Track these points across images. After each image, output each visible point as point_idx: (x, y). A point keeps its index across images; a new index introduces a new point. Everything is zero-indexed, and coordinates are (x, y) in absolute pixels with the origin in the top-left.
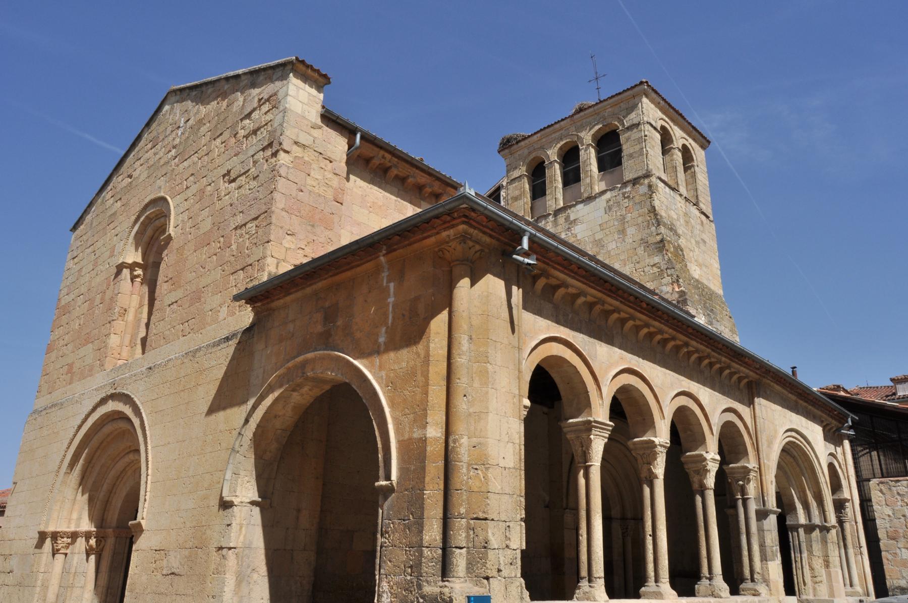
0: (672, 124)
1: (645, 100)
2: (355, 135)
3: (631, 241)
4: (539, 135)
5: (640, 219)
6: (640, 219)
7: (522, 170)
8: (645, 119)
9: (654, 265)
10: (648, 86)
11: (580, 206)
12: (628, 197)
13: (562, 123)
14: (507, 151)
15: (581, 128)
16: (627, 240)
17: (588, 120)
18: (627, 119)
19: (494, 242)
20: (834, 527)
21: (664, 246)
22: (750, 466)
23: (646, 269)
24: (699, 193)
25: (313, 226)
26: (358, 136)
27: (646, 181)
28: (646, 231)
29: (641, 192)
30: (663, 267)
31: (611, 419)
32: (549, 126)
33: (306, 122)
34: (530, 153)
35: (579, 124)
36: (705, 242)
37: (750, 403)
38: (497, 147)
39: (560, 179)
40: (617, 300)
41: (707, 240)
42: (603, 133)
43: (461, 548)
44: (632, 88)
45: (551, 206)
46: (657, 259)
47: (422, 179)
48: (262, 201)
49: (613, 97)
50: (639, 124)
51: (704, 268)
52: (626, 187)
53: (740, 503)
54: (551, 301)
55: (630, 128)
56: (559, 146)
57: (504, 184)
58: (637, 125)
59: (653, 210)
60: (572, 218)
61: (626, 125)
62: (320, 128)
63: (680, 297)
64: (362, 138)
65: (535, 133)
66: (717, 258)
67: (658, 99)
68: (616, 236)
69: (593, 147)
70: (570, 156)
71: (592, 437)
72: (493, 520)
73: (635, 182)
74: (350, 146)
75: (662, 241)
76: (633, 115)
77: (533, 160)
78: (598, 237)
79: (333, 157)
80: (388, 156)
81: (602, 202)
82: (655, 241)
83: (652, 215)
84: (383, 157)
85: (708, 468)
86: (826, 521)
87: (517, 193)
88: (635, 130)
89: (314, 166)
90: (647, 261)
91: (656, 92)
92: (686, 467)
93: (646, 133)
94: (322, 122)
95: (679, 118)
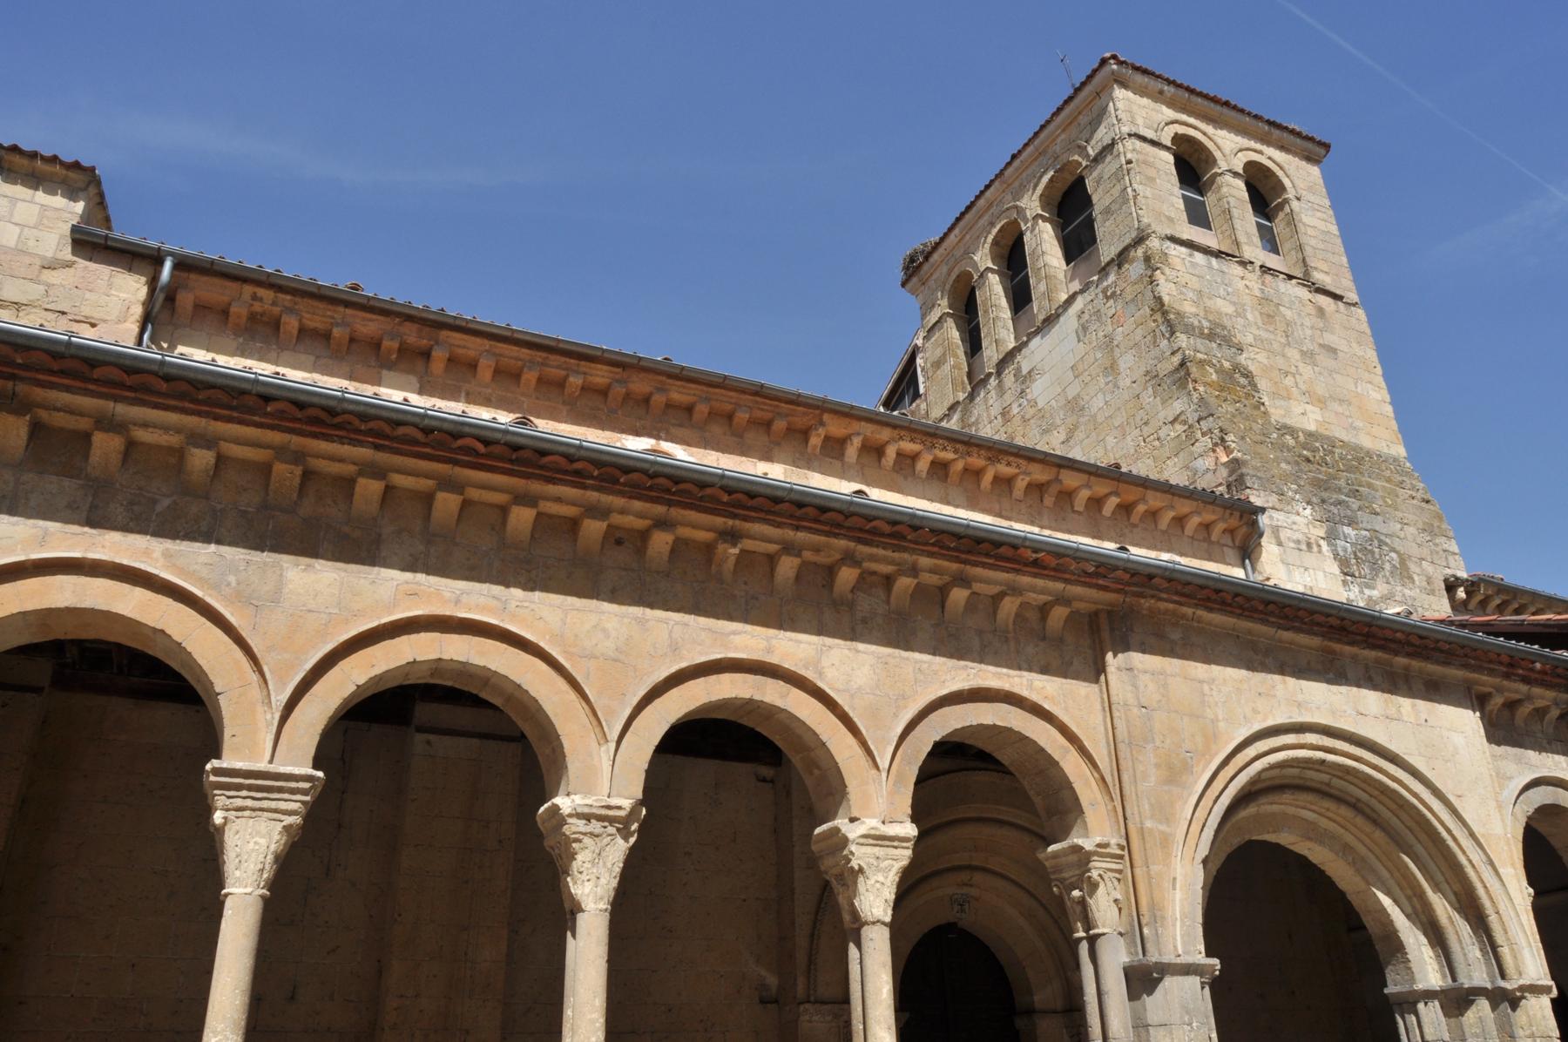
0: (1210, 129)
1: (1119, 93)
3: (1128, 382)
4: (956, 231)
5: (1139, 331)
6: (1139, 331)
7: (943, 306)
8: (1125, 130)
9: (1175, 420)
10: (1121, 63)
11: (1036, 341)
13: (988, 194)
15: (1018, 196)
16: (1121, 384)
17: (1029, 171)
18: (1093, 142)
20: (1536, 990)
21: (1188, 374)
22: (1088, 844)
23: (1162, 434)
24: (1308, 251)
26: (168, 265)
27: (1140, 252)
30: (1192, 417)
32: (969, 208)
33: (27, 260)
35: (1017, 184)
36: (1332, 351)
37: (1096, 671)
38: (901, 275)
39: (1004, 302)
40: (361, 444)
41: (1341, 345)
42: (1062, 187)
44: (1090, 77)
45: (990, 358)
46: (1178, 406)
47: (369, 326)
49: (1059, 110)
50: (1113, 143)
51: (1336, 406)
52: (1107, 275)
53: (1084, 948)
55: (1098, 159)
56: (990, 238)
57: (919, 342)
58: (1109, 148)
59: (1159, 306)
60: (1025, 371)
61: (1091, 152)
62: (69, 265)
63: (1231, 473)
64: (177, 266)
65: (951, 229)
66: (1380, 380)
67: (1159, 85)
68: (1102, 380)
69: (1045, 220)
70: (1013, 258)
71: (218, 817)
73: (1121, 259)
74: (153, 283)
75: (1182, 364)
76: (1102, 131)
78: (1071, 393)
79: (96, 314)
81: (1069, 321)
82: (1171, 368)
83: (1158, 316)
84: (255, 297)
85: (854, 864)
86: (1503, 976)
87: (939, 352)
88: (1109, 158)
90: (1161, 415)
91: (1145, 72)
93: (1129, 156)
94: (74, 254)
95: (1225, 110)
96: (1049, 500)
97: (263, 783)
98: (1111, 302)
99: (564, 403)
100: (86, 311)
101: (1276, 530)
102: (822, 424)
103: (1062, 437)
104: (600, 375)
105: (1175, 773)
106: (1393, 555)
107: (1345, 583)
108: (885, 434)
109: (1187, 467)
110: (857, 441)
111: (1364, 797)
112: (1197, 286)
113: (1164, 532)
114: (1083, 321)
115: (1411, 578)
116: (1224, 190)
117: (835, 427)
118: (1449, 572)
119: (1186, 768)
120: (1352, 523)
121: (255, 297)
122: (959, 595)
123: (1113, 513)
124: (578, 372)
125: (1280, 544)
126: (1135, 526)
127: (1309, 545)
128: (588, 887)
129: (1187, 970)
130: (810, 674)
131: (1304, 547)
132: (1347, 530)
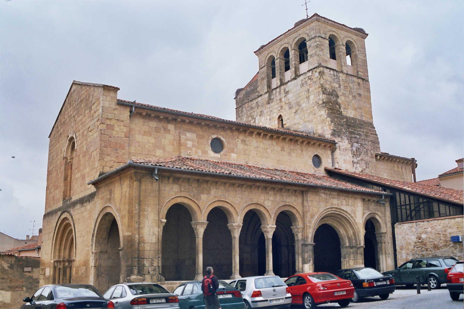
2: (132, 108)
3: (312, 103)
5: (315, 91)
6: (315, 91)
25: (116, 150)
26: (134, 108)
28: (318, 97)
29: (316, 76)
31: (207, 221)
33: (111, 109)
43: (136, 266)
51: (358, 110)
62: (117, 109)
64: (135, 108)
68: (306, 100)
72: (146, 258)
89: (116, 126)
97: (202, 223)
98: (310, 80)
100: (121, 119)
101: (339, 147)
105: (312, 217)
107: (353, 157)
112: (330, 80)
114: (302, 83)
115: (368, 155)
116: (340, 50)
118: (377, 152)
119: (314, 215)
120: (357, 143)
128: (237, 235)
129: (311, 245)
130: (263, 204)
131: (345, 150)
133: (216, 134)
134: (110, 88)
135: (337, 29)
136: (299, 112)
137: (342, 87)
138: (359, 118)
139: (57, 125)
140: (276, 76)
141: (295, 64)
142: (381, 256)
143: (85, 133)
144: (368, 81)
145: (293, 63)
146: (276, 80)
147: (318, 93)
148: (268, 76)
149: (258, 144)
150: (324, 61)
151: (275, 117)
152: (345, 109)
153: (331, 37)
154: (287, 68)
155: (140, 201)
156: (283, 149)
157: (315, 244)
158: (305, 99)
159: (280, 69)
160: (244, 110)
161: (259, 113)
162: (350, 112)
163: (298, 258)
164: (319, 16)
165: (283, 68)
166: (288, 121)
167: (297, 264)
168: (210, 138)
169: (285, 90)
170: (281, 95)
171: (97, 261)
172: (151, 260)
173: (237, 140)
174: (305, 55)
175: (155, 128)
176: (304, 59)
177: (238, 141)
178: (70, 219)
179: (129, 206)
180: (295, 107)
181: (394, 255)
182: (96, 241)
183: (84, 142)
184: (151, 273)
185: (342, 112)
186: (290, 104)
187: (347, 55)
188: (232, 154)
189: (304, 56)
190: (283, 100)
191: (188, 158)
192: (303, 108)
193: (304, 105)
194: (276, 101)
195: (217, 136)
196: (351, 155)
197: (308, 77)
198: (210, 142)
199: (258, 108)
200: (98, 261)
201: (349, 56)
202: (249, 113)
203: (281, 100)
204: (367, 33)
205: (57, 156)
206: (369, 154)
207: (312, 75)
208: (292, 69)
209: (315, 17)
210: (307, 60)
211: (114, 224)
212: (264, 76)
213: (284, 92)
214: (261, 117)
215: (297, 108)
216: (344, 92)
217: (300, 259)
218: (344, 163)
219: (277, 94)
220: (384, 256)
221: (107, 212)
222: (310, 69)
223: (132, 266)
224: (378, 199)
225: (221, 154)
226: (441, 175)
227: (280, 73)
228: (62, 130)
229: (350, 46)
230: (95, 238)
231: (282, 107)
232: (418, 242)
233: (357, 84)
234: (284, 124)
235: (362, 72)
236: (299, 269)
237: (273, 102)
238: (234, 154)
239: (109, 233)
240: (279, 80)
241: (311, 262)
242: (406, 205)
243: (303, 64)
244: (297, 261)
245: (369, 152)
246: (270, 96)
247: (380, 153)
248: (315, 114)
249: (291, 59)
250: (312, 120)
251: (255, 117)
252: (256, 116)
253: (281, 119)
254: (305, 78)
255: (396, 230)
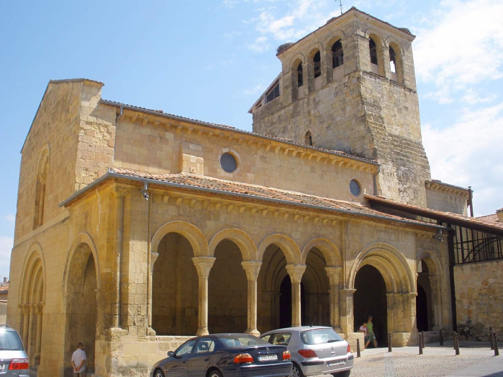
12: (347, 86)
13: (310, 36)
14: (281, 55)
19: (133, 186)
29: (353, 83)
34: (294, 56)
36: (406, 108)
38: (276, 52)
48: (87, 142)
54: (174, 205)
59: (360, 95)
68: (340, 112)
72: (131, 304)
77: (295, 62)
80: (141, 114)
84: (138, 115)
92: (287, 271)
96: (325, 162)
98: (346, 88)
99: (208, 139)
101: (383, 170)
102: (271, 144)
103: (326, 126)
104: (217, 132)
106: (413, 175)
108: (286, 146)
109: (362, 146)
110: (279, 148)
111: (389, 257)
112: (371, 88)
113: (354, 170)
114: (336, 91)
117: (274, 144)
118: (427, 179)
120: (404, 166)
121: (138, 115)
122: (317, 219)
123: (342, 165)
124: (212, 132)
125: (383, 174)
126: (347, 169)
127: (391, 174)
131: (390, 175)
132: (402, 168)
133: (228, 148)
134: (92, 83)
135: (379, 28)
136: (332, 127)
137: (385, 97)
138: (406, 136)
139: (30, 137)
140: (304, 83)
141: (327, 68)
142: (435, 307)
143: (60, 142)
144: (415, 92)
145: (325, 67)
146: (304, 88)
147: (356, 104)
148: (293, 83)
149: (282, 162)
150: (364, 65)
151: (302, 134)
152: (388, 124)
153: (371, 37)
154: (317, 75)
155: (123, 226)
156: (313, 170)
157: (356, 290)
158: (340, 110)
159: (309, 75)
160: (263, 125)
161: (282, 130)
162: (395, 128)
163: (334, 308)
164: (357, 10)
165: (313, 74)
166: (319, 138)
167: (332, 316)
168: (220, 152)
169: (314, 100)
170: (310, 106)
171: (69, 306)
172: (137, 306)
173: (255, 156)
174: (340, 58)
175: (149, 136)
176: (338, 63)
177: (256, 158)
178: (40, 252)
179: (108, 232)
180: (328, 120)
181: (452, 305)
182: (68, 281)
183: (59, 154)
184: (137, 324)
185: (386, 128)
186: (321, 118)
187: (391, 61)
188: (248, 173)
189: (339, 59)
190: (312, 112)
191: (190, 177)
192: (337, 122)
193: (338, 119)
194: (304, 114)
195: (229, 149)
196: (397, 181)
197: (344, 84)
198: (220, 157)
199: (280, 123)
200: (71, 307)
201: (392, 62)
202: (268, 129)
203: (309, 112)
204: (414, 34)
205: (28, 175)
206: (418, 181)
207: (348, 82)
208: (324, 75)
209: (353, 11)
210: (342, 63)
211: (91, 260)
212: (288, 84)
213: (314, 103)
214: (284, 134)
215: (330, 122)
216: (389, 104)
217: (337, 310)
218: (389, 190)
219: (305, 105)
220: (439, 306)
221: (82, 242)
222: (346, 74)
223: (111, 315)
224: (434, 234)
225: (233, 174)
226: (500, 211)
227: (309, 79)
228: (34, 143)
229: (395, 50)
230: (67, 277)
231: (310, 121)
232: (485, 289)
233: (403, 95)
234: (313, 142)
235: (409, 81)
236: (334, 323)
237: (299, 115)
238: (250, 174)
239: (85, 271)
240: (307, 88)
241: (350, 313)
242: (468, 242)
243: (337, 68)
244: (332, 312)
245: (418, 179)
246: (295, 107)
247: (430, 180)
248: (352, 130)
249: (323, 62)
250: (348, 137)
251: (276, 134)
252: (278, 133)
253: (309, 137)
254: (340, 86)
255: (455, 274)
